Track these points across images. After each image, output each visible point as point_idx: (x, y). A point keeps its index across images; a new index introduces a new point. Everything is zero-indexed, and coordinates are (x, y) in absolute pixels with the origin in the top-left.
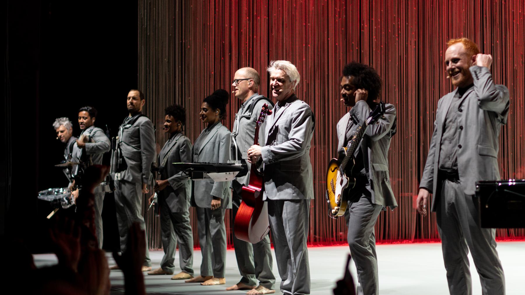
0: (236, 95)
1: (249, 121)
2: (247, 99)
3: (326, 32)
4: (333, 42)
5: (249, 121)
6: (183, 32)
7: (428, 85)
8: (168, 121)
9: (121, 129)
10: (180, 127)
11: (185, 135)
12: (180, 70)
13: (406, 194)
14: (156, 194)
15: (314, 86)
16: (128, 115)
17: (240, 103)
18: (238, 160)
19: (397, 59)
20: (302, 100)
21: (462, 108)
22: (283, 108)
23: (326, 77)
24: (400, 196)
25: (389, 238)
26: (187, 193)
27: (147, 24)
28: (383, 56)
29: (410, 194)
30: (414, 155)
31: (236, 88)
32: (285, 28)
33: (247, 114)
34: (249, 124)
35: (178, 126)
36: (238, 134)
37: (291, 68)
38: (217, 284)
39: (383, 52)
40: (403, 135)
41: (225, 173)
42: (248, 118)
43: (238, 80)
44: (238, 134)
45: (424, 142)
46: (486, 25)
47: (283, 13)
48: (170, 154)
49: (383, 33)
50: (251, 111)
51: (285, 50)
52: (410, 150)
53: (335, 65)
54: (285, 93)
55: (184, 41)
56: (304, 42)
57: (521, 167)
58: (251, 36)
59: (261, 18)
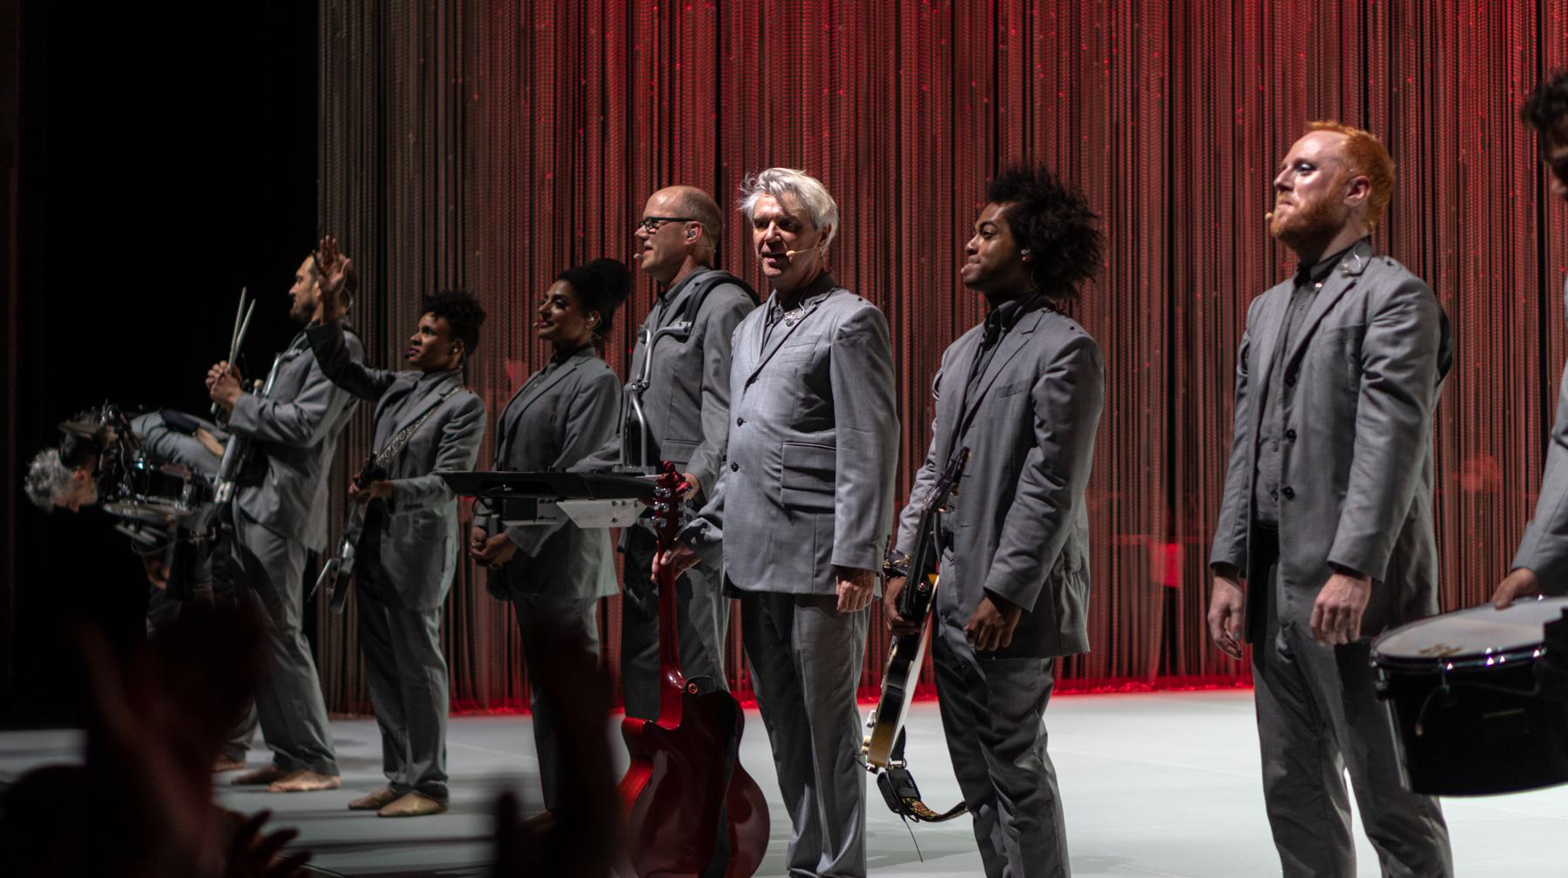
0: (646, 263)
1: (683, 348)
2: (678, 280)
3: (892, 52)
4: (914, 82)
5: (683, 348)
8: (426, 330)
12: (451, 167)
13: (1133, 540)
15: (857, 214)
17: (662, 294)
18: (649, 464)
19: (1107, 131)
20: (857, 292)
22: (794, 316)
23: (892, 186)
24: (1115, 542)
25: (1080, 674)
27: (349, 28)
28: (1064, 124)
29: (1143, 537)
30: (1156, 424)
31: (648, 243)
32: (767, 39)
33: (679, 325)
34: (683, 357)
35: (451, 353)
36: (648, 385)
37: (809, 186)
39: (1064, 111)
40: (1123, 365)
41: (609, 502)
42: (681, 338)
43: (654, 220)
44: (648, 385)
45: (1186, 385)
49: (1065, 54)
50: (691, 317)
51: (767, 106)
52: (1145, 410)
53: (921, 153)
54: (801, 268)
57: (1477, 458)
58: (666, 62)
59: (694, 9)
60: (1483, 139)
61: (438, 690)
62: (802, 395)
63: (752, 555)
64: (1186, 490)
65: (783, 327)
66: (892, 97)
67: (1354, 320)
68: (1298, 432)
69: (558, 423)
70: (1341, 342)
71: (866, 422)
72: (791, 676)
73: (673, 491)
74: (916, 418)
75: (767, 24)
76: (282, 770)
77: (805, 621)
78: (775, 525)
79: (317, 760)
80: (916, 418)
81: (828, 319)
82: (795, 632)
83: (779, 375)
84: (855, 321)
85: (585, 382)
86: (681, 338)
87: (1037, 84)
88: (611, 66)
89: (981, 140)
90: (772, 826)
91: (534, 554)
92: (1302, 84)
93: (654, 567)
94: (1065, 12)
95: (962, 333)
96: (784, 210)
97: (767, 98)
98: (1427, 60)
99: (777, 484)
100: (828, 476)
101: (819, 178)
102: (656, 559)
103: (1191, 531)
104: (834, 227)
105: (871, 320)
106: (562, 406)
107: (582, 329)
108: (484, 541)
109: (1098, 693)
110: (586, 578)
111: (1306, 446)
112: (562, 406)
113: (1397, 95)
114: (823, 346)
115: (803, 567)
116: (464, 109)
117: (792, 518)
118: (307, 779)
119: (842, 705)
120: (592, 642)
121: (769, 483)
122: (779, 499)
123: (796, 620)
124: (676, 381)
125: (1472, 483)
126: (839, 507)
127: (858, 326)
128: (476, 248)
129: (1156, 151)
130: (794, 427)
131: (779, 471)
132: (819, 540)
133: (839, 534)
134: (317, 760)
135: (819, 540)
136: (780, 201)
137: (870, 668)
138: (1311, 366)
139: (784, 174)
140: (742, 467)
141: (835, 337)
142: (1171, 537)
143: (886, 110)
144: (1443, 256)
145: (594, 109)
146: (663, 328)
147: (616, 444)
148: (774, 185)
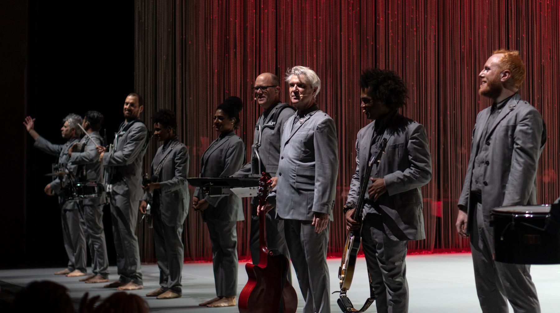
1: (273, 132)
3: (338, 26)
4: (346, 37)
5: (273, 132)
6: (184, 27)
7: (448, 83)
9: (116, 136)
10: (171, 132)
11: (183, 142)
14: (149, 205)
16: (124, 121)
21: (490, 142)
22: (302, 120)
26: (185, 204)
32: (294, 22)
33: (271, 124)
34: (273, 135)
36: (260, 145)
37: (310, 73)
38: (225, 306)
39: (400, 47)
41: (249, 188)
42: (272, 128)
44: (260, 145)
45: (444, 145)
46: (511, 18)
47: (292, 5)
48: (165, 163)
49: (400, 26)
55: (184, 37)
56: (315, 37)
57: (548, 170)
58: (258, 30)
60: (550, 56)
61: (180, 255)
62: (303, 149)
63: (286, 206)
64: (444, 182)
65: (298, 124)
66: (339, 43)
67: (512, 123)
68: (490, 162)
69: (223, 159)
70: (507, 130)
71: (326, 160)
72: (301, 250)
73: (265, 183)
74: (347, 157)
75: (294, 16)
76: (124, 281)
77: (305, 230)
78: (293, 195)
79: (136, 279)
80: (347, 157)
81: (314, 122)
82: (302, 233)
83: (296, 142)
84: (323, 123)
85: (232, 144)
86: (272, 128)
87: (390, 38)
88: (237, 32)
89: (370, 58)
90: (299, 302)
91: (215, 206)
92: (485, 37)
93: (258, 211)
94: (400, 11)
95: (364, 127)
96: (300, 81)
97: (294, 43)
98: (530, 28)
99: (294, 181)
100: (312, 178)
101: (313, 69)
102: (258, 208)
103: (446, 197)
104: (319, 88)
105: (328, 123)
106: (224, 153)
107: (230, 125)
108: (197, 202)
109: (412, 254)
110: (234, 213)
111: (492, 167)
112: (224, 153)
113: (519, 41)
114: (311, 132)
115: (303, 210)
116: (186, 47)
117: (300, 193)
118: (130, 285)
119: (321, 259)
120: (234, 237)
121: (292, 181)
122: (295, 186)
123: (302, 229)
124: (271, 144)
125: (546, 179)
126: (316, 190)
127: (324, 125)
128: (190, 96)
129: (433, 61)
130: (300, 161)
131: (295, 176)
132: (309, 201)
133: (315, 200)
134: (136, 279)
135: (309, 201)
136: (299, 78)
137: (331, 246)
138: (496, 139)
139: (302, 68)
140: (282, 175)
141: (315, 129)
142: (439, 199)
143: (336, 47)
144: (536, 98)
145: (232, 47)
146: (266, 124)
147: (249, 166)
148: (297, 72)
